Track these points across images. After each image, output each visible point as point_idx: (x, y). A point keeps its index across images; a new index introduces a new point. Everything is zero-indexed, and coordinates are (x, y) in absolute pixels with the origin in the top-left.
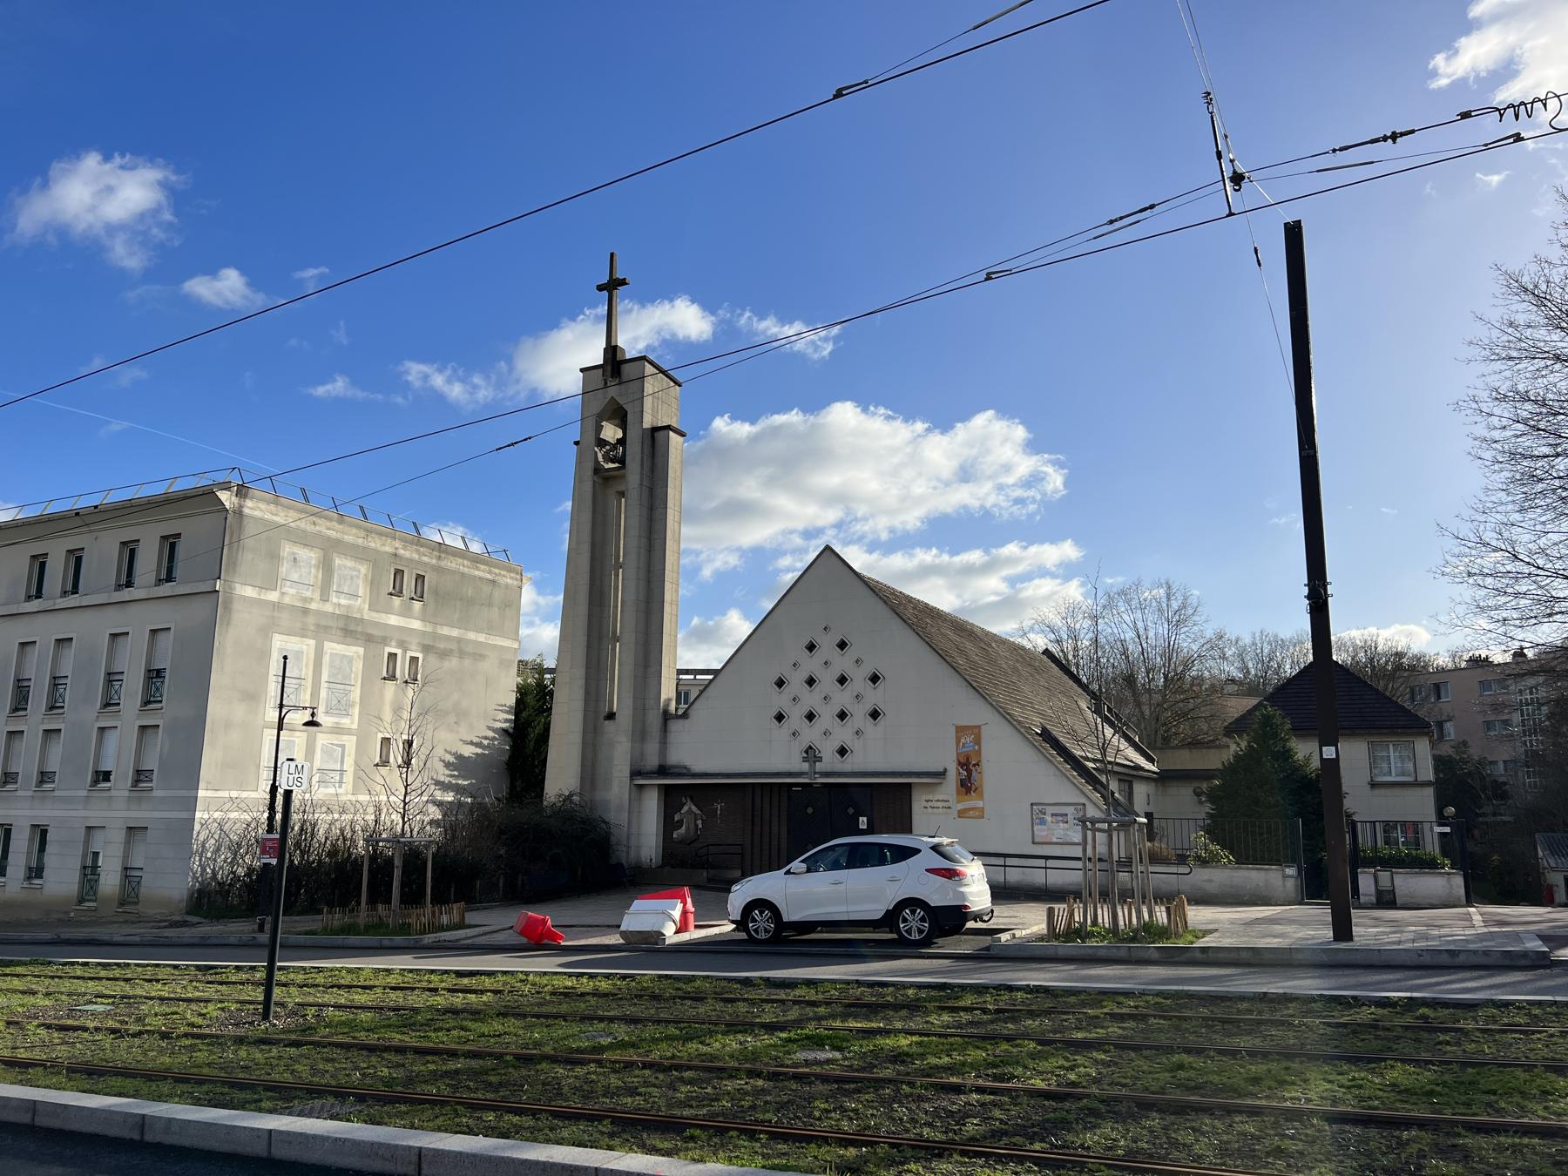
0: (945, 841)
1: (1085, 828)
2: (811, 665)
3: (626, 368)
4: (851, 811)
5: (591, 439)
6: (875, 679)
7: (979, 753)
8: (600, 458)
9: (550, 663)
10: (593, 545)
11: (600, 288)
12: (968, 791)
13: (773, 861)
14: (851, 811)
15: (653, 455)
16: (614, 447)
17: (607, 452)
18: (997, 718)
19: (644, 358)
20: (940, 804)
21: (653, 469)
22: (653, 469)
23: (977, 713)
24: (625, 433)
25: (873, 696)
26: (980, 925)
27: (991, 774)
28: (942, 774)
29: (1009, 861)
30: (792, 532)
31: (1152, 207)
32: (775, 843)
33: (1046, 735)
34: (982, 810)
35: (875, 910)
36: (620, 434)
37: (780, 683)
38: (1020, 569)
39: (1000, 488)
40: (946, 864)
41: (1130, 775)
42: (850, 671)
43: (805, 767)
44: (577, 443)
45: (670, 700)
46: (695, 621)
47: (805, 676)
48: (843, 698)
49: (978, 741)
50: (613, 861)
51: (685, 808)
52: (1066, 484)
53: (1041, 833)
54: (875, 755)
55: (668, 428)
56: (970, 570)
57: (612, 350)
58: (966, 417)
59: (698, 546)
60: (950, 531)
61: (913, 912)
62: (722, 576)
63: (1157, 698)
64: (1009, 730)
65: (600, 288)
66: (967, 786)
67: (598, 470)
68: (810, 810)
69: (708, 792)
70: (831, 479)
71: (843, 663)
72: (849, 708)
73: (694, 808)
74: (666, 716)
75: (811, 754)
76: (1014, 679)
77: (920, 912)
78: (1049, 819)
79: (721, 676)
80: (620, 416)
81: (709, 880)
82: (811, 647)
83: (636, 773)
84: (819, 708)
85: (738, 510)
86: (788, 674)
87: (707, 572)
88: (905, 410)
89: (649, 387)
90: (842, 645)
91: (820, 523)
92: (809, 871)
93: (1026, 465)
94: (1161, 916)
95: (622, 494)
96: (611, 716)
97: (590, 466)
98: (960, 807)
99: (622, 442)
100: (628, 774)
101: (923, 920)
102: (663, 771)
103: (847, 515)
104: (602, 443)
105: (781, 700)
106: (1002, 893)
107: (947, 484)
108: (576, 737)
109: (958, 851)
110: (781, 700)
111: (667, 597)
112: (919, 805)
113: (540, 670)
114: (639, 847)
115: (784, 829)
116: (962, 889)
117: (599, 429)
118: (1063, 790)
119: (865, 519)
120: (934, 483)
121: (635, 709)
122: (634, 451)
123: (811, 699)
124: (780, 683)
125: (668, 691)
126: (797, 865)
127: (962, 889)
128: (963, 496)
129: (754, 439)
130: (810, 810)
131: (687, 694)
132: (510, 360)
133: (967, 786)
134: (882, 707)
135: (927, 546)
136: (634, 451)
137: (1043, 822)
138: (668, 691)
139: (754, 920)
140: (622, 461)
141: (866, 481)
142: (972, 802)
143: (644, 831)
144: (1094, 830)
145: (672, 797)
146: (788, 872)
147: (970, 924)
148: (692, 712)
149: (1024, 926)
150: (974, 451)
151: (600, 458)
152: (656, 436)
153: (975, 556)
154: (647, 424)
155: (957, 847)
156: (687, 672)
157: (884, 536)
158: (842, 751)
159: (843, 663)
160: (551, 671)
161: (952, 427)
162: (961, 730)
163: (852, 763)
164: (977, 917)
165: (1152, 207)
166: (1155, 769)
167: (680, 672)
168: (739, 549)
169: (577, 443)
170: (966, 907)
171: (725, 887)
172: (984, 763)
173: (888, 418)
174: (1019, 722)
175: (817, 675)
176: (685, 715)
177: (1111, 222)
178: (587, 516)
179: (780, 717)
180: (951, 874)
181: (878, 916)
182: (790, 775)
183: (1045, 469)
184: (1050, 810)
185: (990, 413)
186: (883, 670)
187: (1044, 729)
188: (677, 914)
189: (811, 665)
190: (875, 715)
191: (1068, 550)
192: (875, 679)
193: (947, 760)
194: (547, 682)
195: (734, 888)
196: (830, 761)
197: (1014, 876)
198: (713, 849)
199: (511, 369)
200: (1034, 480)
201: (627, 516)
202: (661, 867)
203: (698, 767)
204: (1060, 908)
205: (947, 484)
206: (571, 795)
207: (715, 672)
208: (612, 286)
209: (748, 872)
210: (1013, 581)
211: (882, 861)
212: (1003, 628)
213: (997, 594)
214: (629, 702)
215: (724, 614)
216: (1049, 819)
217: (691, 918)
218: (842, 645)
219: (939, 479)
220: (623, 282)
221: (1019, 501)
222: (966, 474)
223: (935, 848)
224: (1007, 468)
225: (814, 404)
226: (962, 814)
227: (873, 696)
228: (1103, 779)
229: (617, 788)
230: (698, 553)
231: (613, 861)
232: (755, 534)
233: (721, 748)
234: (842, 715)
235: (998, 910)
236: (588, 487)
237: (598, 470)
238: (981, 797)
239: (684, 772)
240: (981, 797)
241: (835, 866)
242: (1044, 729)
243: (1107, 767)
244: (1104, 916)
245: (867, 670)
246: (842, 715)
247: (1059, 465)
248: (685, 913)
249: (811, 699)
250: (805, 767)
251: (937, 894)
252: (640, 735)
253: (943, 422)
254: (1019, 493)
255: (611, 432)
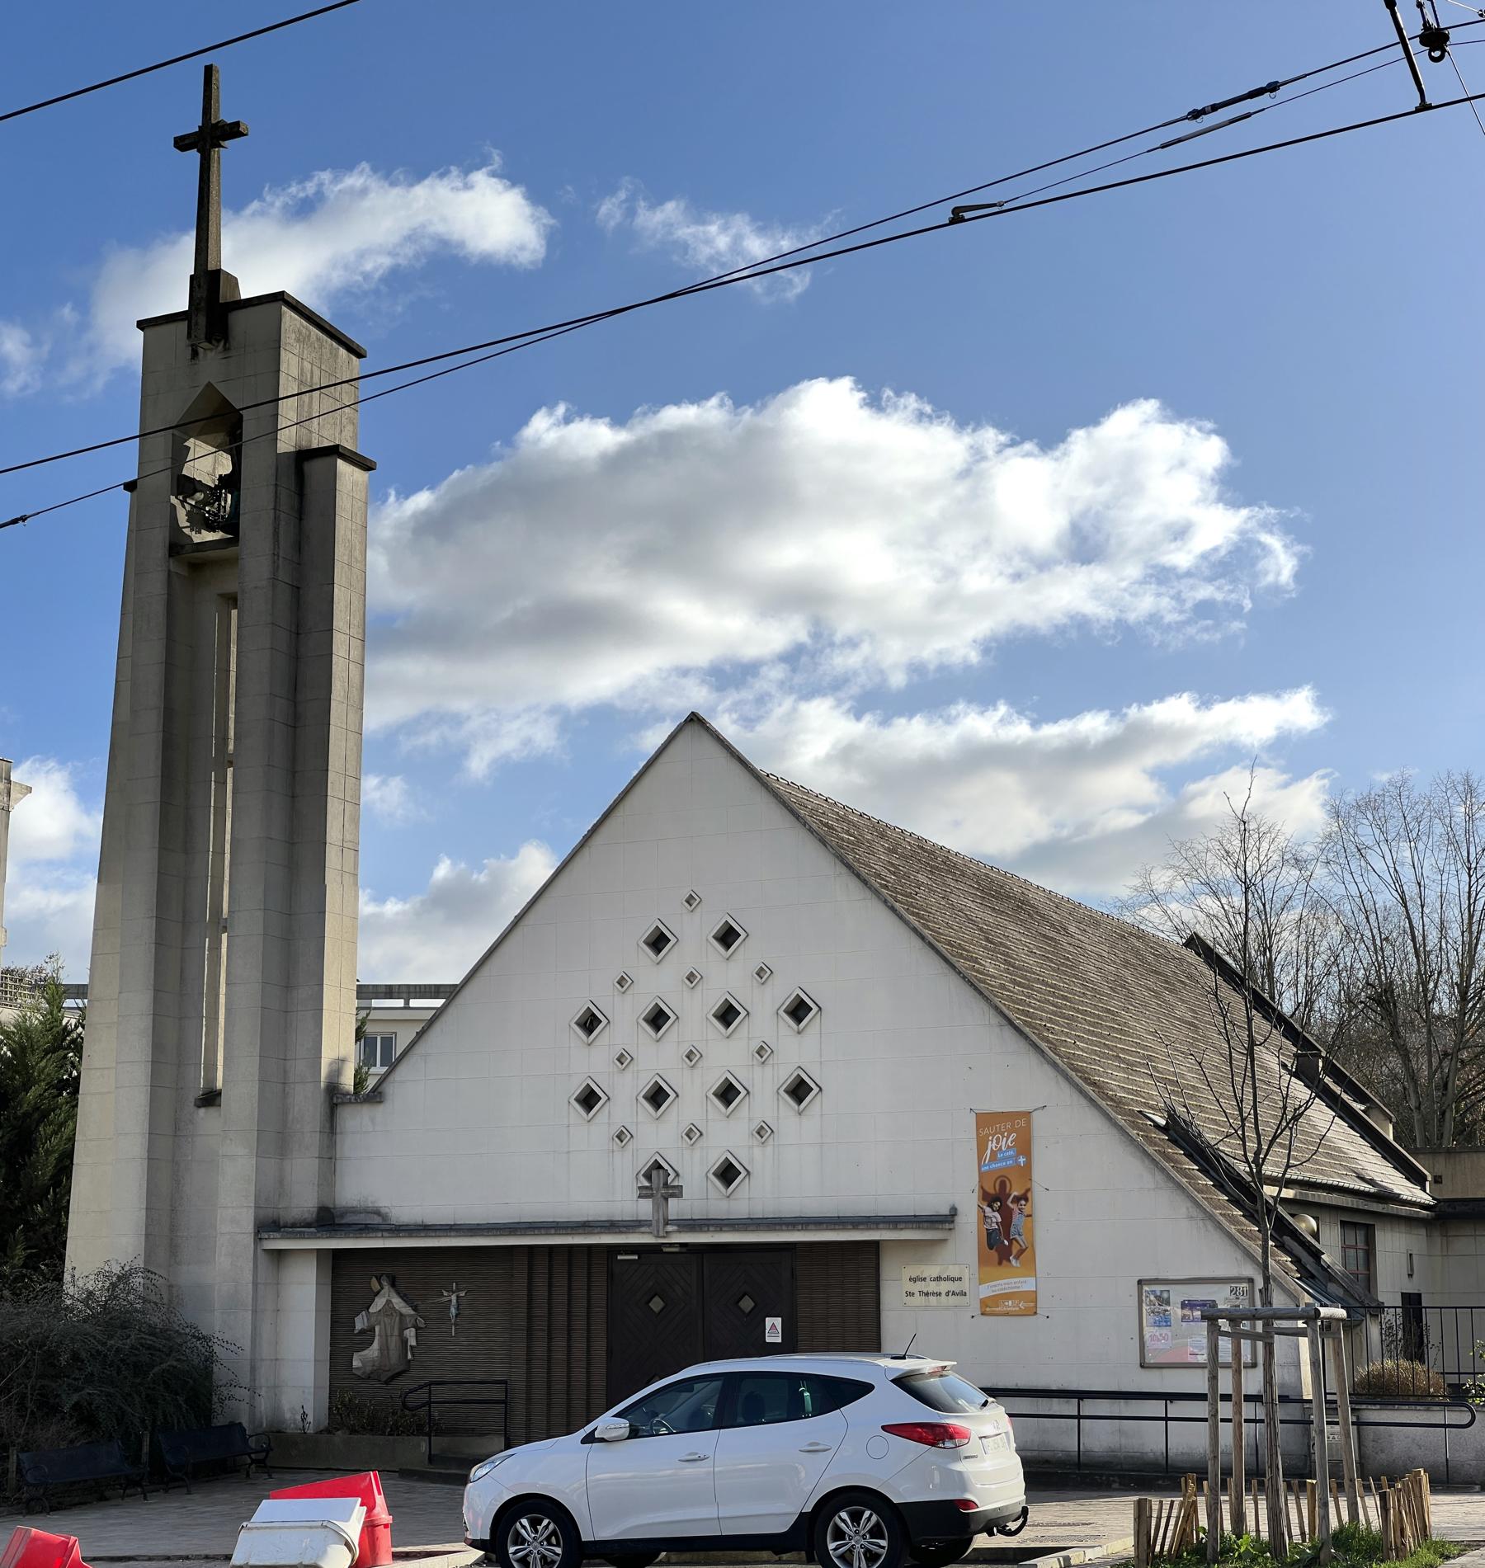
0: (927, 1365)
1: (1215, 1332)
2: (658, 981)
3: (238, 319)
4: (747, 1304)
5: (164, 480)
6: (798, 1010)
7: (1026, 1171)
8: (183, 521)
9: (75, 972)
10: (169, 714)
11: (182, 143)
12: (1004, 1256)
13: (564, 1417)
14: (747, 1304)
15: (300, 513)
16: (214, 494)
17: (199, 506)
18: (1066, 1094)
19: (280, 298)
20: (944, 1287)
21: (299, 545)
22: (299, 545)
23: (1021, 1082)
24: (237, 464)
25: (797, 1051)
26: (999, 1541)
27: (1050, 1220)
28: (946, 1220)
29: (1089, 1407)
30: (684, 672)
31: (1273, 87)
32: (579, 1374)
33: (1179, 1133)
34: (1033, 1297)
35: (776, 1514)
36: (225, 466)
37: (589, 1023)
38: (1185, 752)
39: (1162, 576)
40: (922, 1414)
41: (1365, 1213)
42: (744, 994)
43: (645, 1209)
44: (130, 486)
45: (342, 1061)
46: (443, 871)
47: (646, 1007)
48: (728, 1055)
49: (1024, 1146)
50: (219, 1421)
51: (379, 1304)
52: (1298, 576)
53: (1161, 1343)
54: (799, 1177)
55: (335, 451)
56: (1078, 756)
57: (209, 282)
58: (1092, 416)
59: (462, 705)
60: (1033, 667)
61: (856, 1517)
62: (509, 772)
63: (1447, 1038)
64: (1092, 1122)
65: (182, 143)
66: (1003, 1245)
67: (177, 546)
68: (657, 1304)
69: (428, 1267)
70: (785, 553)
71: (728, 977)
72: (742, 1076)
73: (397, 1302)
74: (334, 1097)
75: (658, 1180)
76: (1114, 1005)
77: (869, 1517)
78: (1176, 1311)
79: (460, 1000)
80: (224, 423)
81: (431, 1459)
82: (658, 942)
83: (267, 1226)
84: (675, 1077)
85: (575, 625)
86: (608, 1003)
87: (479, 764)
88: (957, 401)
89: (292, 365)
90: (727, 937)
91: (750, 652)
92: (634, 1434)
93: (1219, 527)
94: (1370, 1511)
95: (232, 600)
96: (211, 1098)
97: (159, 539)
98: (986, 1291)
99: (230, 482)
100: (250, 1228)
101: (876, 1532)
102: (327, 1220)
103: (816, 636)
104: (186, 486)
105: (591, 1062)
106: (1049, 1476)
107: (1043, 565)
108: (134, 1145)
109: (962, 1388)
110: (591, 1062)
111: (333, 833)
112: (899, 1292)
113: (54, 992)
114: (276, 1389)
115: (600, 1346)
116: (959, 1467)
117: (180, 455)
118: (1208, 1253)
119: (852, 643)
120: (1018, 564)
121: (263, 1081)
122: (258, 500)
123: (658, 1059)
124: (589, 1023)
125: (337, 1043)
126: (608, 1423)
127: (959, 1467)
128: (1071, 594)
129: (617, 463)
130: (657, 1304)
131: (388, 1042)
132: (84, 303)
133: (1003, 1245)
134: (815, 1073)
135: (984, 699)
136: (258, 500)
137: (1164, 1321)
138: (337, 1043)
139: (519, 1540)
140: (231, 525)
141: (856, 557)
142: (1012, 1282)
143: (286, 1355)
144: (1236, 1336)
145: (348, 1277)
146: (590, 1439)
147: (981, 1541)
148: (389, 1088)
149: (1084, 1543)
150: (1105, 491)
151: (183, 521)
152: (309, 471)
153: (1094, 725)
154: (287, 442)
155: (953, 1378)
156: (390, 992)
157: (898, 680)
158: (728, 1173)
159: (728, 977)
160: (80, 991)
161: (1062, 438)
162: (987, 1122)
163: (757, 1196)
164: (994, 1524)
165: (1273, 87)
166: (1424, 1197)
167: (365, 992)
168: (556, 710)
169: (130, 486)
170: (968, 1504)
171: (454, 1473)
172: (1038, 1195)
173: (921, 416)
174: (1118, 1103)
175: (673, 1003)
176: (376, 1096)
177: (1196, 114)
178: (153, 652)
179: (589, 1099)
180: (935, 1435)
181: (781, 1527)
182: (612, 1226)
183: (1266, 538)
184: (1177, 1294)
185: (1150, 407)
186: (816, 990)
187: (1172, 1116)
188: (353, 1528)
189: (658, 981)
190: (799, 1090)
191: (1298, 710)
192: (798, 1010)
193: (960, 1189)
194: (69, 1020)
195: (477, 1472)
196: (699, 1194)
197: (1062, 1438)
198: (441, 1393)
199: (84, 326)
200: (1236, 561)
201: (241, 652)
202: (328, 1431)
203: (404, 1210)
204: (1166, 1508)
205: (1043, 565)
206: (124, 1278)
207: (449, 993)
208: (209, 136)
209: (516, 1434)
210: (1174, 779)
211: (795, 1412)
212: (1104, 890)
213: (1142, 809)
214: (250, 1066)
215: (513, 853)
216: (1176, 1311)
217: (385, 1537)
218: (727, 937)
219: (1025, 553)
220: (234, 131)
221: (1204, 609)
222: (1085, 544)
223: (904, 1382)
224: (1180, 532)
225: (760, 380)
226: (988, 1307)
227: (797, 1051)
228: (1307, 1224)
229: (224, 1259)
230: (457, 720)
231: (219, 1421)
232: (603, 676)
233: (503, 1153)
234: (727, 1093)
235: (1037, 1513)
236: (156, 584)
237: (177, 546)
238: (1031, 1268)
239: (373, 1221)
240: (1031, 1268)
241: (695, 1423)
242: (1172, 1116)
243: (1315, 1198)
244: (1296, 1512)
245: (782, 992)
246: (727, 1093)
247: (1291, 529)
248: (370, 1527)
249: (658, 1059)
250: (645, 1209)
251: (907, 1477)
252: (275, 1139)
253: (1043, 425)
254: (1205, 592)
255: (207, 463)
